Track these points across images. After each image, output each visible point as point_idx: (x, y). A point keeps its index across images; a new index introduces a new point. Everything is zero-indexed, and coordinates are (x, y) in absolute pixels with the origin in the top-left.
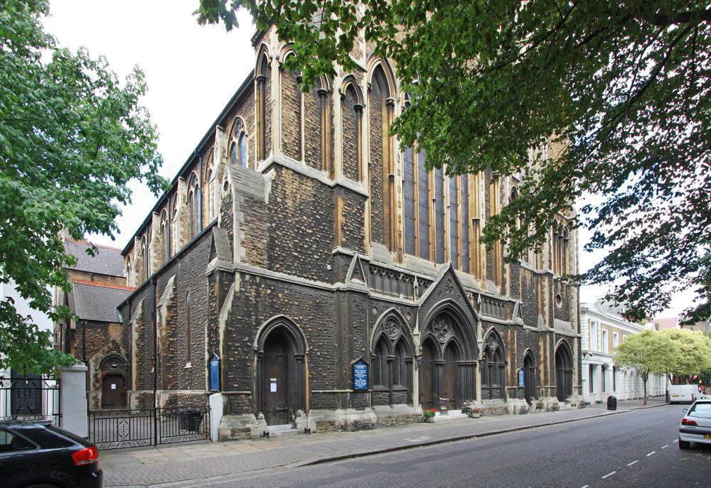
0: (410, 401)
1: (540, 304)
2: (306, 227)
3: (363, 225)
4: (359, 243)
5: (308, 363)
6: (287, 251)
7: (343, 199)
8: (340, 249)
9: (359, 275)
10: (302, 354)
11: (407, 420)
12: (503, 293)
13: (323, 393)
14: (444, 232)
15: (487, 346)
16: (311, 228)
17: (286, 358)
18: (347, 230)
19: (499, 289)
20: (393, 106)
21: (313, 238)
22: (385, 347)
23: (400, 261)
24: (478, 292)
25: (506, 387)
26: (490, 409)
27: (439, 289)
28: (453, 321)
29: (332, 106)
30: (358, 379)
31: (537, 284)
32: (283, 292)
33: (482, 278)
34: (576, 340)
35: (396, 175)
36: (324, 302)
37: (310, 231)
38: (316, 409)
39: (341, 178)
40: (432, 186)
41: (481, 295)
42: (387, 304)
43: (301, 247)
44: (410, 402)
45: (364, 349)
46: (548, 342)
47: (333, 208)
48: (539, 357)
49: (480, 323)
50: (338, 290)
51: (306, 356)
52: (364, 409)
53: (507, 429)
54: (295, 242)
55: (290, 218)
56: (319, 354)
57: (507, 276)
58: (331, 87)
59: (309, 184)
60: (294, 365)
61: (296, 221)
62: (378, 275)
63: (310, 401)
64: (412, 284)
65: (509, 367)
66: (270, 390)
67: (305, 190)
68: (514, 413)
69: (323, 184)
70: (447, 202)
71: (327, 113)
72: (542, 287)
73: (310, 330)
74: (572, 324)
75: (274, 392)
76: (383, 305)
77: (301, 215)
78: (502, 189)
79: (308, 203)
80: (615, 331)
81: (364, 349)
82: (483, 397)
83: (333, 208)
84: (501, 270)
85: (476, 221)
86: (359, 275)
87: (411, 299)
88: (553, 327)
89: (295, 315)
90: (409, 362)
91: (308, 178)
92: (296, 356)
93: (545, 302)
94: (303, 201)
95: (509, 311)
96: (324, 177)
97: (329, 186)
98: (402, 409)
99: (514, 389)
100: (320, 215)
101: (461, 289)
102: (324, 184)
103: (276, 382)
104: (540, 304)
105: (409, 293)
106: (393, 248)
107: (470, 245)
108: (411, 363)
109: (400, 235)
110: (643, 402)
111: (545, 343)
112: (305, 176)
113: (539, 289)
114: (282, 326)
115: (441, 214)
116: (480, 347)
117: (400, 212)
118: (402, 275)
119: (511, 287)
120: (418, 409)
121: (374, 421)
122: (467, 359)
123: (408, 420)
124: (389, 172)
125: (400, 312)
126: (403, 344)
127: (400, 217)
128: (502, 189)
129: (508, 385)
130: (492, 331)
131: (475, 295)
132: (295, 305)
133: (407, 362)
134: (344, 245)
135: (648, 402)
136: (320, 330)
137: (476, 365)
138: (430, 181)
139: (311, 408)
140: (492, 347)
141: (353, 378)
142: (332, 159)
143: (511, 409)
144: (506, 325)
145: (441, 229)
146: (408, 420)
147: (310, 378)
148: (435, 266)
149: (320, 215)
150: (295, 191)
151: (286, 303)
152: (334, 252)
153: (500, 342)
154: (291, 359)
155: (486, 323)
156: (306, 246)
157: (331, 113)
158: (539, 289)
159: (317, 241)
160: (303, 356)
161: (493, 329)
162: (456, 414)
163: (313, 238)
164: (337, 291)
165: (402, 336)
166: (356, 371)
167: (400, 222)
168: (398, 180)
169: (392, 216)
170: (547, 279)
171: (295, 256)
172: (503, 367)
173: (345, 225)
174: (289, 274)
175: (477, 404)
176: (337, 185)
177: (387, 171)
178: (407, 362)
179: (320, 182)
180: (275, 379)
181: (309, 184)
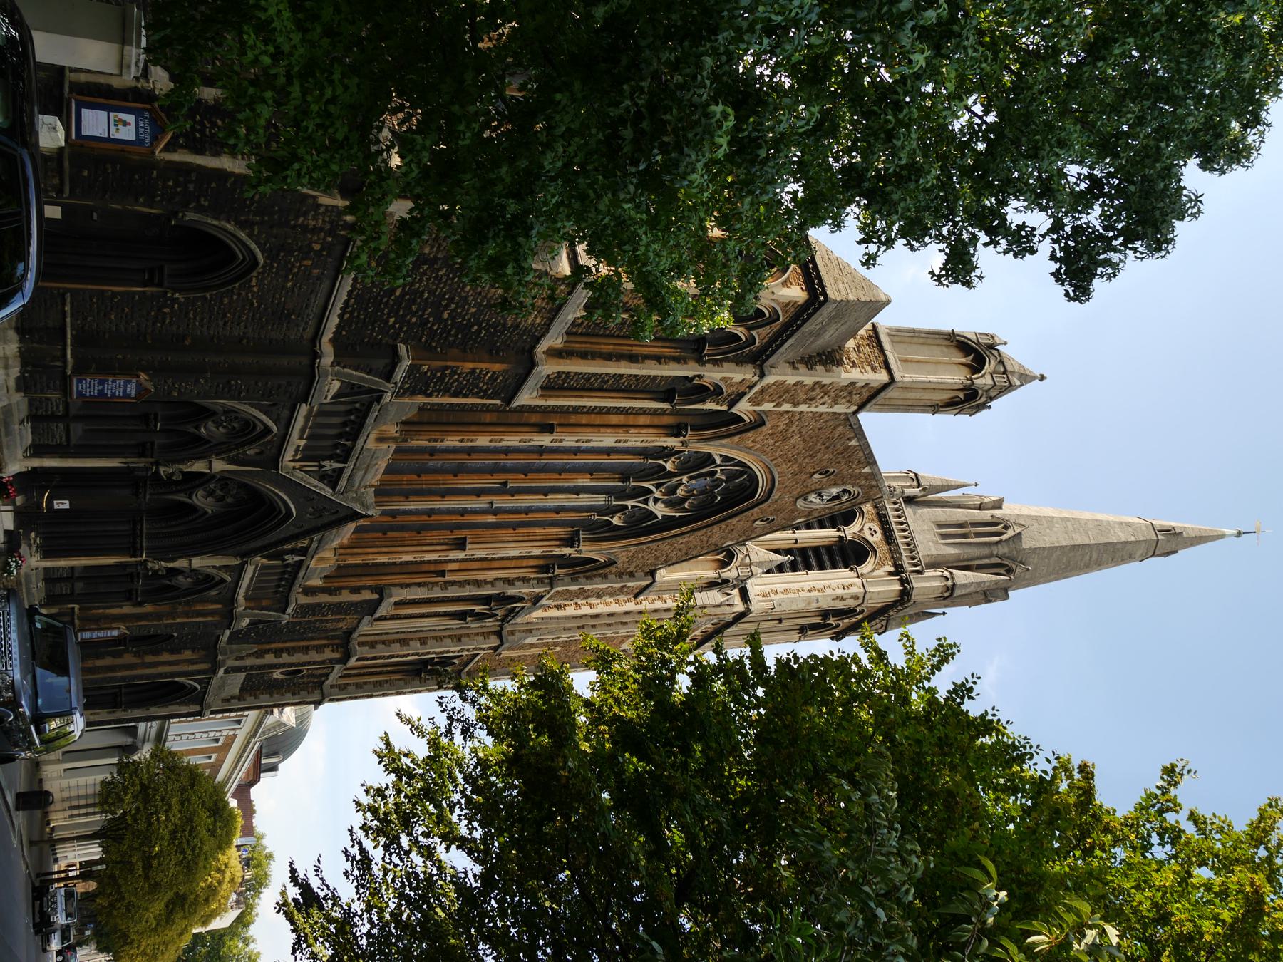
0: (37, 450)
1: (281, 645)
2: (455, 310)
4: (417, 383)
8: (406, 362)
12: (309, 591)
13: (64, 313)
14: (443, 496)
15: (215, 413)
16: (452, 317)
19: (316, 582)
20: (677, 436)
23: (380, 440)
24: (309, 556)
25: (77, 607)
29: (677, 360)
31: (327, 638)
32: (314, 266)
34: (197, 708)
35: (555, 436)
37: (446, 315)
39: (547, 368)
40: (533, 480)
42: (283, 422)
46: (191, 668)
47: (491, 351)
48: (156, 653)
49: (238, 561)
50: (316, 356)
54: (423, 292)
57: (346, 597)
58: (708, 361)
59: (538, 320)
61: (466, 297)
64: (330, 458)
65: (127, 609)
70: (501, 502)
71: (666, 352)
72: (319, 649)
73: (226, 301)
74: (233, 697)
75: (63, 212)
77: (479, 305)
78: (525, 580)
80: (217, 760)
83: (491, 351)
84: (359, 584)
85: (461, 545)
87: (295, 455)
88: (226, 672)
89: (260, 282)
90: (142, 450)
93: (285, 655)
95: (265, 603)
96: (554, 339)
97: (534, 347)
100: (479, 332)
102: (537, 340)
104: (281, 645)
105: (308, 455)
106: (406, 428)
107: (414, 534)
108: (141, 455)
109: (436, 440)
110: (35, 838)
111: (192, 662)
112: (555, 316)
113: (316, 643)
115: (478, 492)
116: (181, 563)
117: (483, 441)
119: (319, 605)
124: (560, 425)
128: (525, 580)
130: (260, 427)
131: (304, 551)
134: (412, 369)
135: (35, 848)
138: (542, 476)
140: (211, 426)
142: (584, 355)
145: (444, 494)
147: (103, 291)
148: (370, 486)
149: (479, 332)
151: (291, 270)
152: (402, 348)
153: (190, 592)
155: (240, 570)
156: (414, 308)
157: (665, 357)
158: (316, 643)
159: (426, 324)
160: (160, 285)
161: (267, 430)
164: (316, 353)
167: (462, 441)
168: (545, 440)
169: (473, 428)
170: (337, 655)
173: (455, 373)
176: (532, 364)
177: (562, 421)
181: (538, 320)
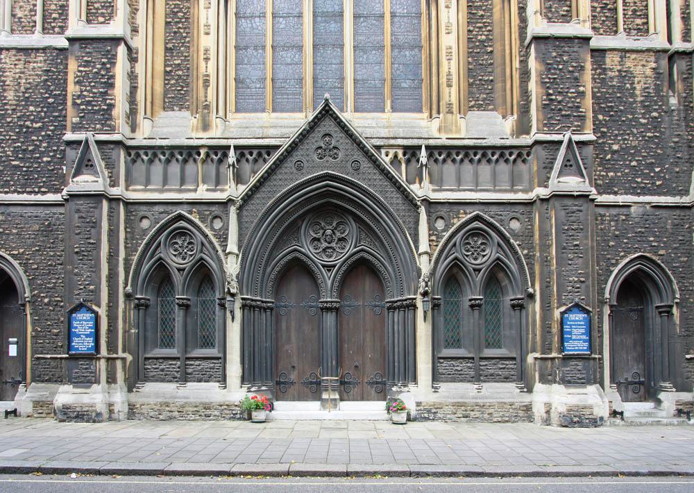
3: (112, 86)
5: (31, 314)
6: (4, 161)
7: (77, 58)
9: (574, 167)
10: (670, 303)
11: (205, 411)
13: (51, 358)
17: (642, 315)
18: (82, 104)
21: (43, 133)
22: (465, 280)
26: (459, 405)
27: (295, 159)
28: (358, 219)
30: (79, 336)
33: (443, 108)
36: (58, 223)
38: (42, 381)
41: (427, 147)
43: (24, 150)
44: (223, 380)
45: (92, 287)
51: (28, 304)
52: (89, 387)
53: (236, 469)
55: (10, 116)
56: (46, 300)
60: (655, 320)
61: (18, 117)
62: (466, 161)
63: (32, 369)
66: (8, 352)
67: (34, 68)
68: (547, 422)
69: (659, 51)
76: (162, 210)
79: (37, 86)
81: (92, 287)
82: (436, 377)
86: (574, 167)
89: (13, 249)
91: (37, 50)
92: (657, 307)
94: (29, 86)
98: (208, 391)
99: (553, 359)
101: (360, 145)
103: (17, 343)
112: (32, 49)
114: (639, 269)
118: (203, 152)
120: (236, 393)
121: (101, 408)
122: (261, 296)
123: (208, 412)
125: (197, 221)
126: (203, 276)
127: (207, 50)
129: (534, 350)
132: (13, 234)
133: (513, 306)
136: (51, 265)
137: (415, 307)
139: (33, 380)
141: (69, 336)
143: (539, 410)
144: (530, 204)
146: (208, 412)
147: (33, 337)
150: (17, 76)
154: (652, 313)
159: (49, 135)
162: (375, 408)
163: (43, 133)
165: (498, 259)
166: (75, 324)
171: (15, 166)
172: (521, 307)
173: (79, 97)
174: (6, 193)
175: (416, 394)
178: (513, 306)
179: (56, 49)
180: (16, 340)
